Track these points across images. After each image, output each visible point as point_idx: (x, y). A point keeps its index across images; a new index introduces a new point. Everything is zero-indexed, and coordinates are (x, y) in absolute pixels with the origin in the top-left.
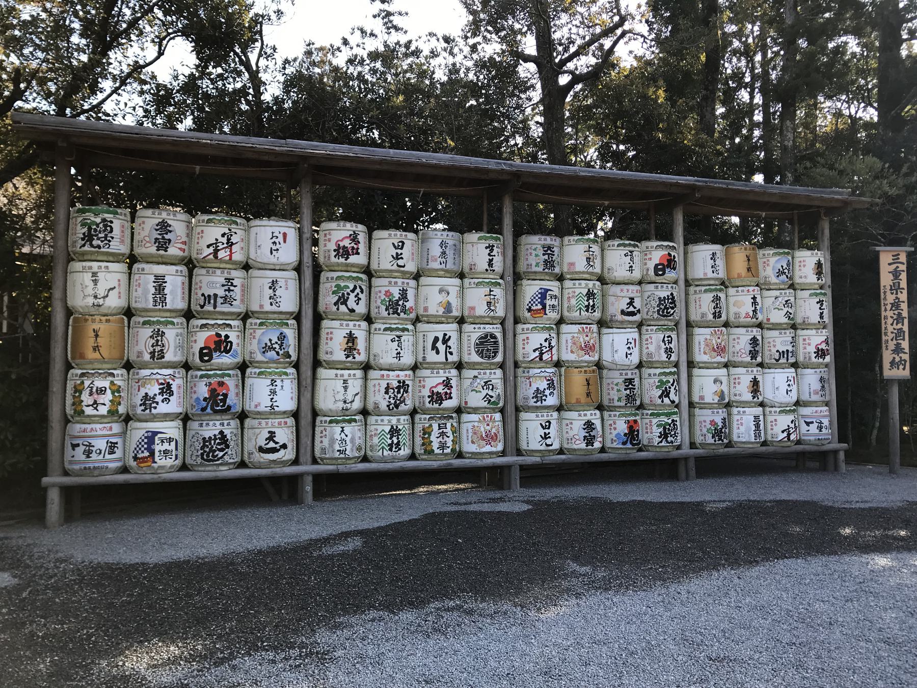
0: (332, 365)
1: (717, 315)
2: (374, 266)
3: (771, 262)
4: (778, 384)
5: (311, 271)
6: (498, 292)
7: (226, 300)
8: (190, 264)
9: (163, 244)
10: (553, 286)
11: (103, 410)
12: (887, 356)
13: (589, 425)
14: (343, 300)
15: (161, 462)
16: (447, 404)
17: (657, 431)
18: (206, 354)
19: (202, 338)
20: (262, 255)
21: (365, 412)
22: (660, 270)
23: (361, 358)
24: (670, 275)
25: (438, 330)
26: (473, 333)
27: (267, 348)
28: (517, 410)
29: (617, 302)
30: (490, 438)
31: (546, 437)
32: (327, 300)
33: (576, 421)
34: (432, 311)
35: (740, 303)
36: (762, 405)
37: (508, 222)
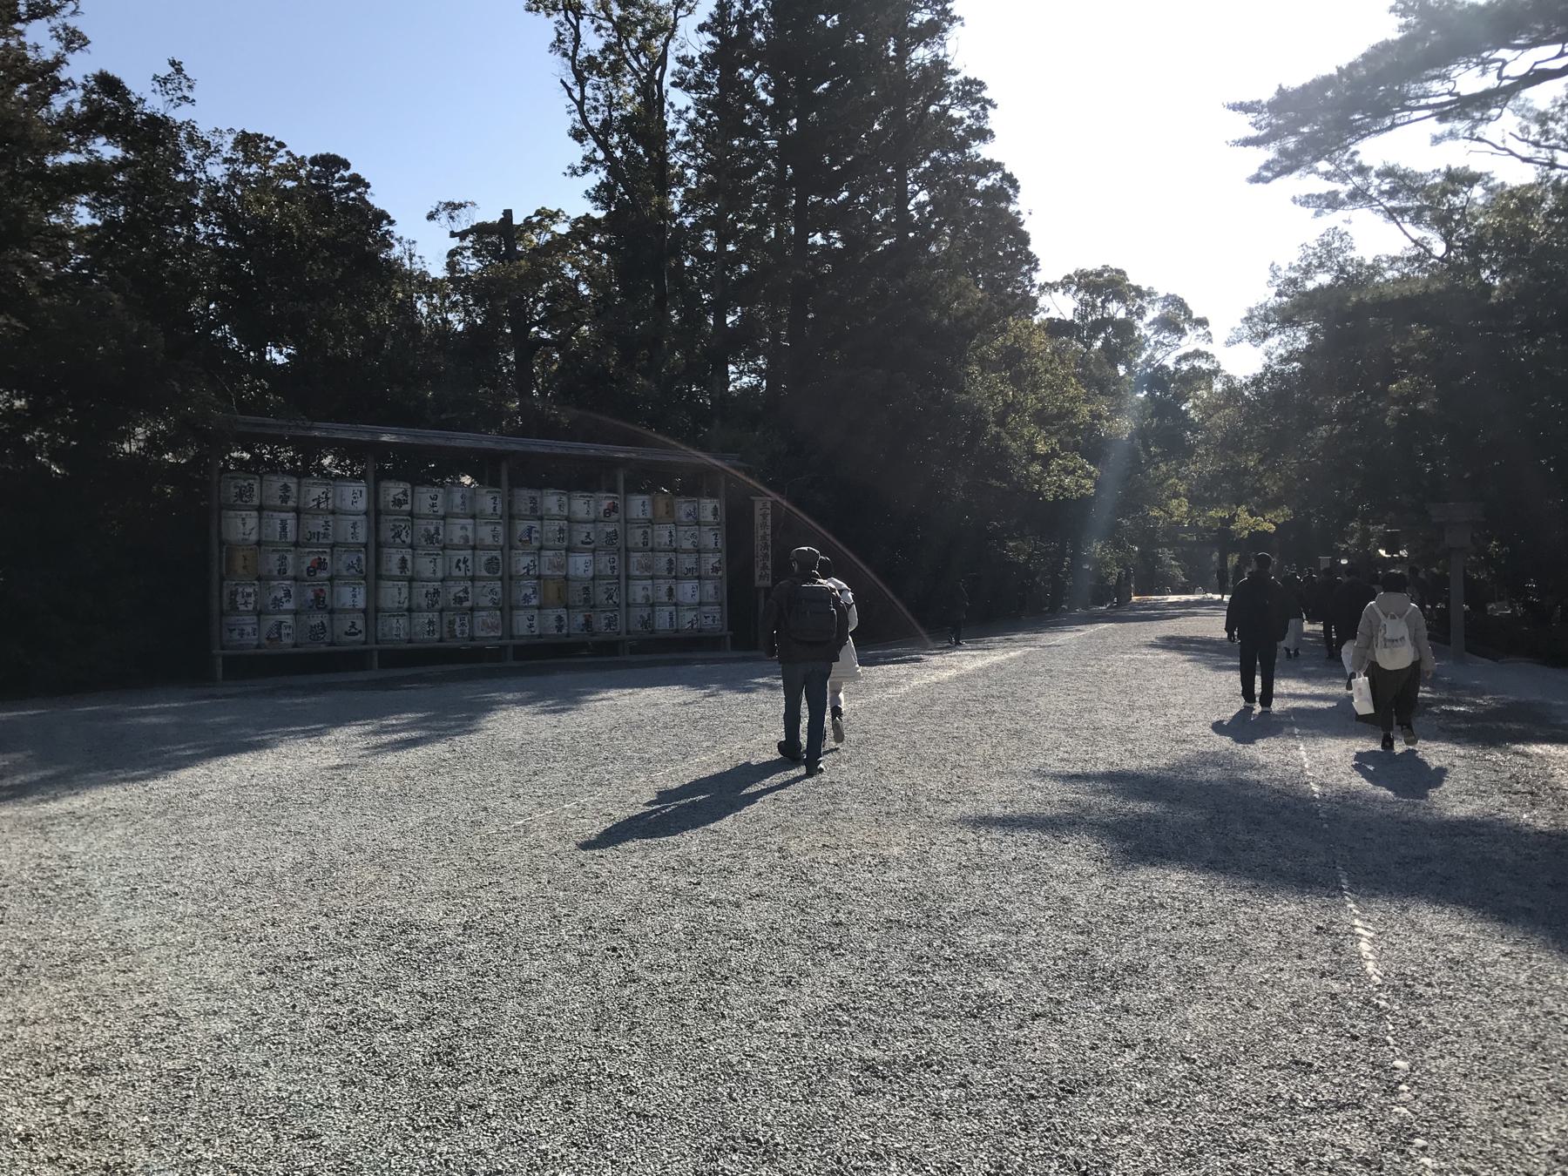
0: (392, 578)
1: (645, 544)
2: (416, 511)
3: (683, 507)
4: (687, 591)
5: (375, 513)
6: (499, 528)
7: (325, 536)
8: (297, 511)
9: (285, 499)
10: (536, 524)
11: (250, 607)
12: (758, 572)
13: (560, 618)
14: (398, 535)
15: (287, 641)
16: (466, 604)
17: (604, 622)
18: (312, 571)
19: (309, 561)
20: (347, 505)
21: (410, 610)
22: (608, 512)
23: (409, 573)
24: (615, 516)
25: (462, 554)
26: (484, 557)
27: (350, 567)
28: (511, 608)
29: (580, 534)
30: (494, 628)
31: (531, 626)
32: (387, 534)
33: (551, 615)
34: (456, 541)
35: (662, 534)
36: (676, 605)
37: (504, 478)
